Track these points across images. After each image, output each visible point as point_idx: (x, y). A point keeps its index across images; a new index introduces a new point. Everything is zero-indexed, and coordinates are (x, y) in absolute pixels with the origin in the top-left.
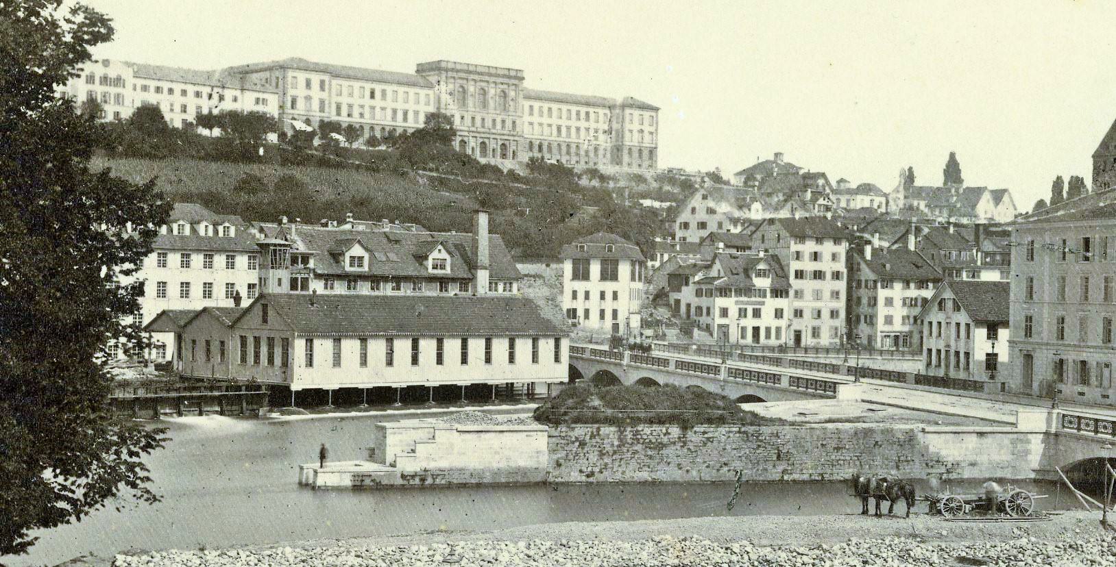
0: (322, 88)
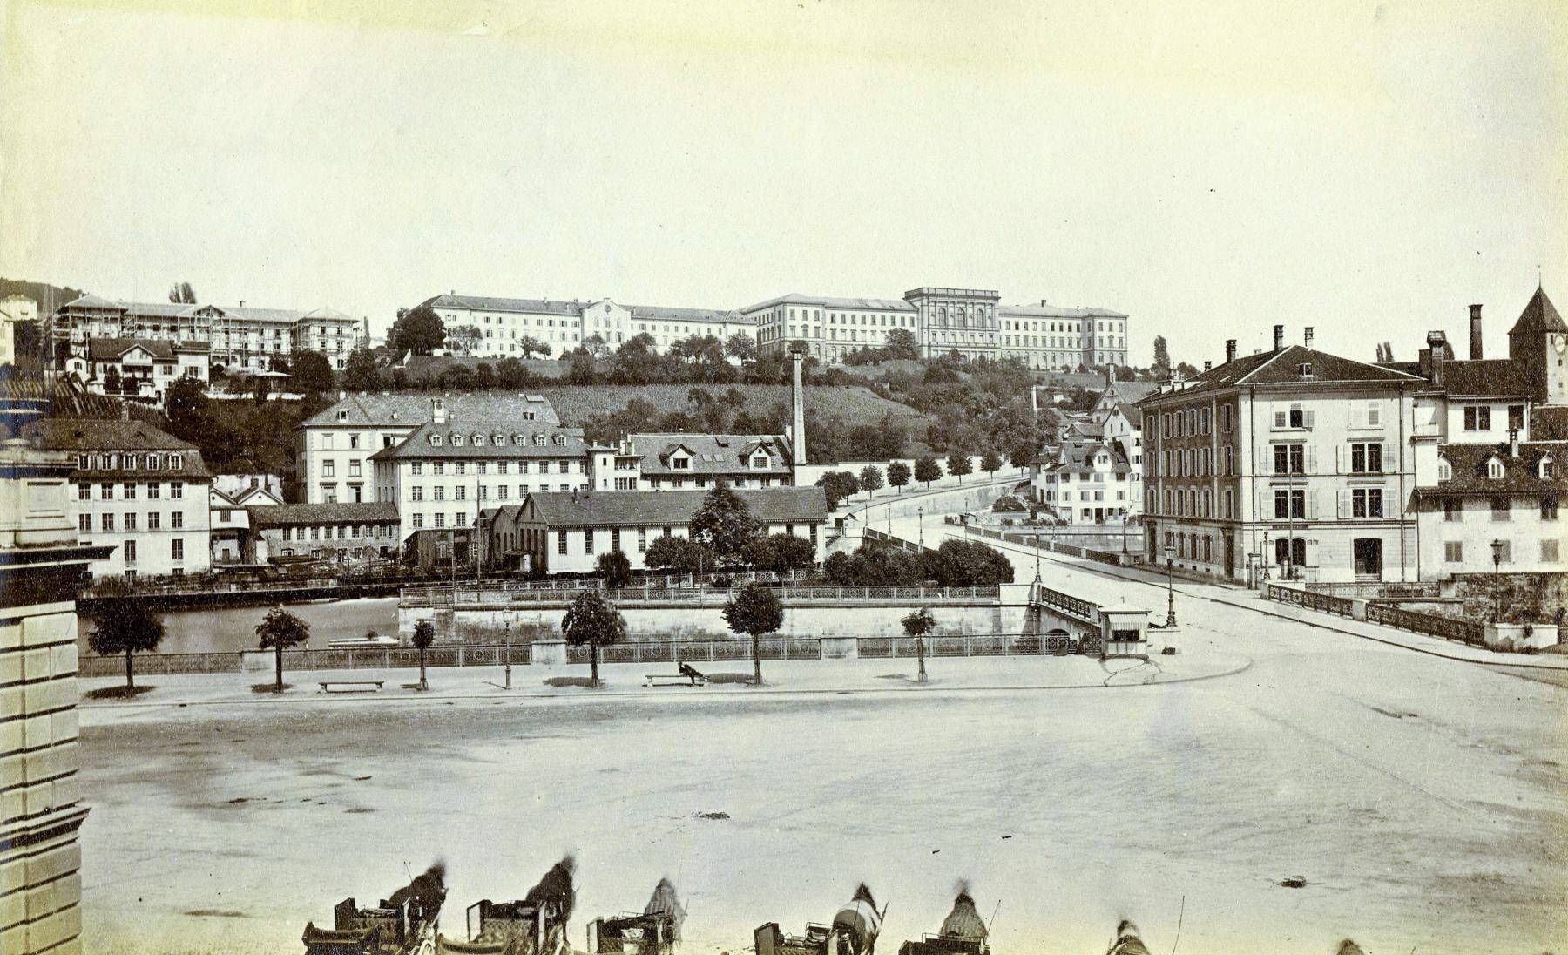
0: (817, 319)
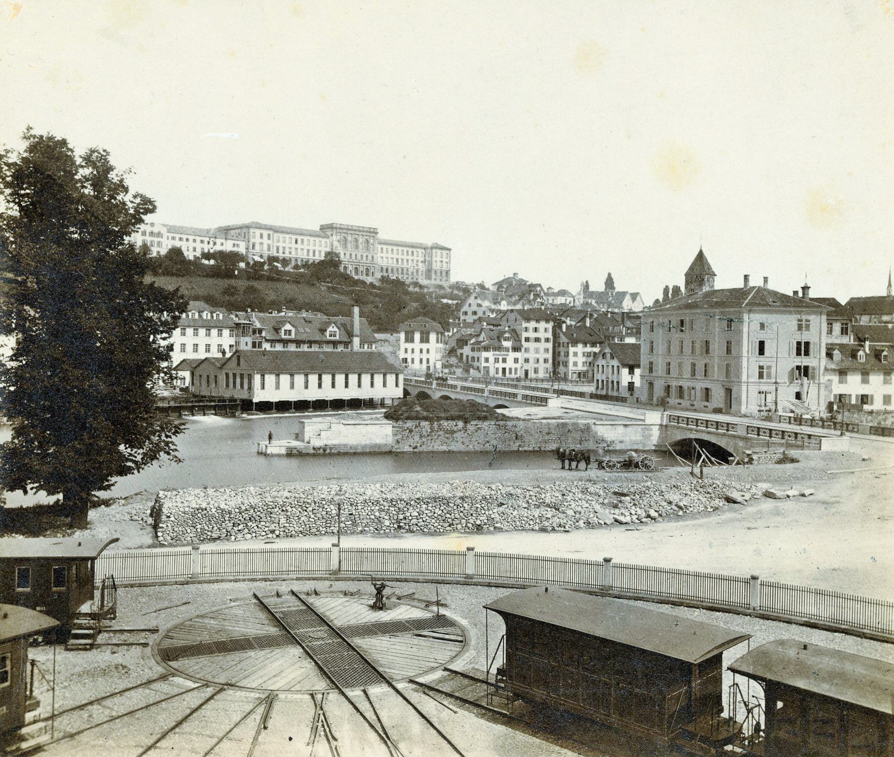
0: (269, 238)
